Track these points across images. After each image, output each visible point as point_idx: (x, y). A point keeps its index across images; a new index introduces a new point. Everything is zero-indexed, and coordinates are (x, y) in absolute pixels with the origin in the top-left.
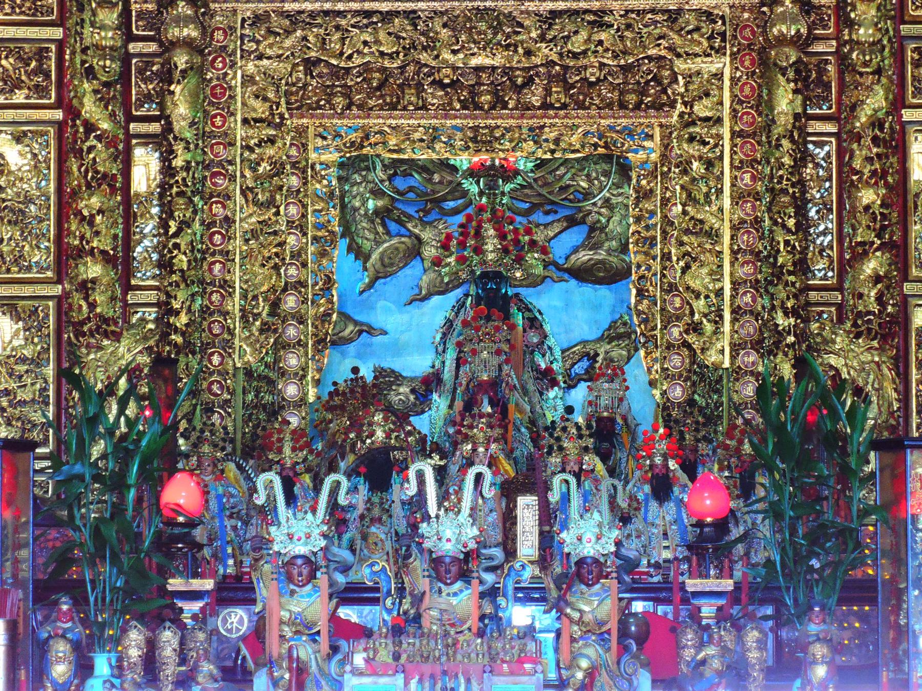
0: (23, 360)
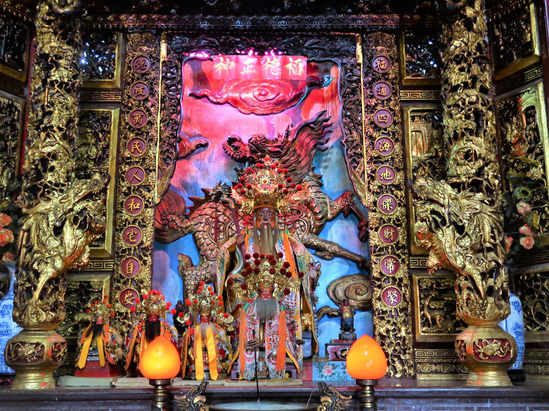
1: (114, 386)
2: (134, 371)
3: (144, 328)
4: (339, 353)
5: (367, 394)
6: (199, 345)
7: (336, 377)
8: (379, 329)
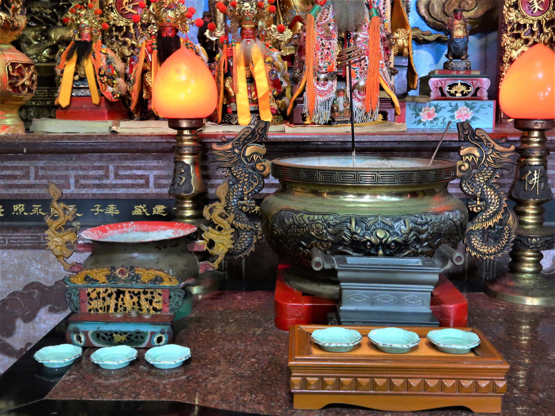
1: (114, 132)
2: (145, 111)
3: (155, 46)
4: (446, 89)
5: (533, 142)
6: (241, 73)
7: (439, 124)
8: (511, 53)
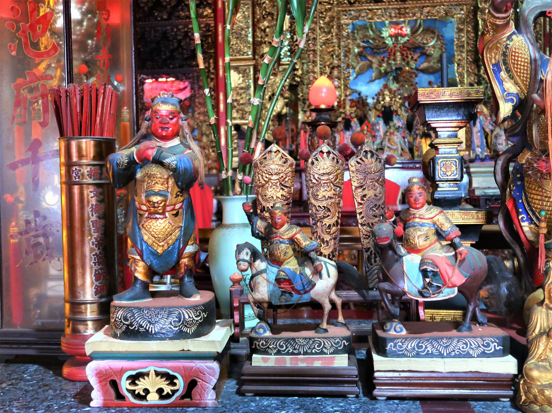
0: (242, 88)
4: (125, 385)
